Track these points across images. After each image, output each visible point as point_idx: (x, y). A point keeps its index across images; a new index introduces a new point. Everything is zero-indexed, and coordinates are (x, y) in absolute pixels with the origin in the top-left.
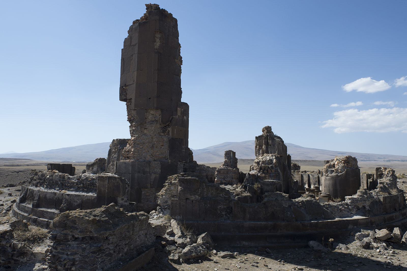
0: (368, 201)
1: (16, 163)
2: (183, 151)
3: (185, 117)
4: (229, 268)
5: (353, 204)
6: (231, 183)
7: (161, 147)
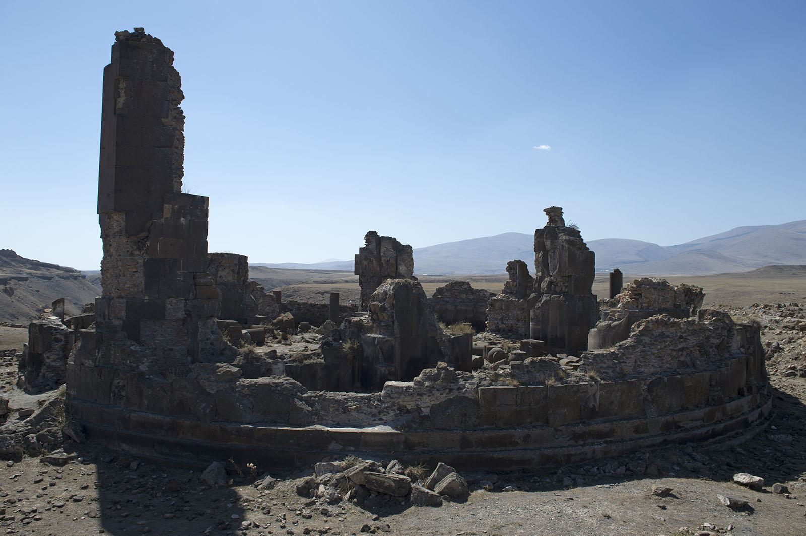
0: (428, 396)
1: (335, 278)
2: (179, 281)
3: (182, 219)
4: (660, 516)
5: (388, 399)
6: (515, 330)
7: (134, 275)
